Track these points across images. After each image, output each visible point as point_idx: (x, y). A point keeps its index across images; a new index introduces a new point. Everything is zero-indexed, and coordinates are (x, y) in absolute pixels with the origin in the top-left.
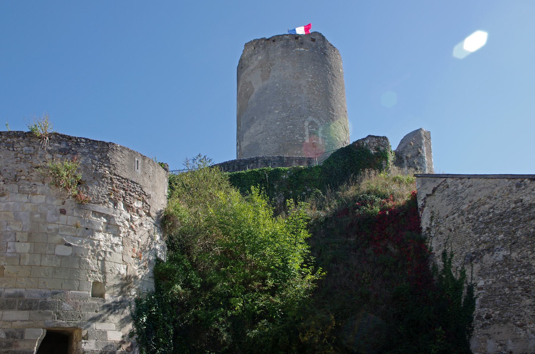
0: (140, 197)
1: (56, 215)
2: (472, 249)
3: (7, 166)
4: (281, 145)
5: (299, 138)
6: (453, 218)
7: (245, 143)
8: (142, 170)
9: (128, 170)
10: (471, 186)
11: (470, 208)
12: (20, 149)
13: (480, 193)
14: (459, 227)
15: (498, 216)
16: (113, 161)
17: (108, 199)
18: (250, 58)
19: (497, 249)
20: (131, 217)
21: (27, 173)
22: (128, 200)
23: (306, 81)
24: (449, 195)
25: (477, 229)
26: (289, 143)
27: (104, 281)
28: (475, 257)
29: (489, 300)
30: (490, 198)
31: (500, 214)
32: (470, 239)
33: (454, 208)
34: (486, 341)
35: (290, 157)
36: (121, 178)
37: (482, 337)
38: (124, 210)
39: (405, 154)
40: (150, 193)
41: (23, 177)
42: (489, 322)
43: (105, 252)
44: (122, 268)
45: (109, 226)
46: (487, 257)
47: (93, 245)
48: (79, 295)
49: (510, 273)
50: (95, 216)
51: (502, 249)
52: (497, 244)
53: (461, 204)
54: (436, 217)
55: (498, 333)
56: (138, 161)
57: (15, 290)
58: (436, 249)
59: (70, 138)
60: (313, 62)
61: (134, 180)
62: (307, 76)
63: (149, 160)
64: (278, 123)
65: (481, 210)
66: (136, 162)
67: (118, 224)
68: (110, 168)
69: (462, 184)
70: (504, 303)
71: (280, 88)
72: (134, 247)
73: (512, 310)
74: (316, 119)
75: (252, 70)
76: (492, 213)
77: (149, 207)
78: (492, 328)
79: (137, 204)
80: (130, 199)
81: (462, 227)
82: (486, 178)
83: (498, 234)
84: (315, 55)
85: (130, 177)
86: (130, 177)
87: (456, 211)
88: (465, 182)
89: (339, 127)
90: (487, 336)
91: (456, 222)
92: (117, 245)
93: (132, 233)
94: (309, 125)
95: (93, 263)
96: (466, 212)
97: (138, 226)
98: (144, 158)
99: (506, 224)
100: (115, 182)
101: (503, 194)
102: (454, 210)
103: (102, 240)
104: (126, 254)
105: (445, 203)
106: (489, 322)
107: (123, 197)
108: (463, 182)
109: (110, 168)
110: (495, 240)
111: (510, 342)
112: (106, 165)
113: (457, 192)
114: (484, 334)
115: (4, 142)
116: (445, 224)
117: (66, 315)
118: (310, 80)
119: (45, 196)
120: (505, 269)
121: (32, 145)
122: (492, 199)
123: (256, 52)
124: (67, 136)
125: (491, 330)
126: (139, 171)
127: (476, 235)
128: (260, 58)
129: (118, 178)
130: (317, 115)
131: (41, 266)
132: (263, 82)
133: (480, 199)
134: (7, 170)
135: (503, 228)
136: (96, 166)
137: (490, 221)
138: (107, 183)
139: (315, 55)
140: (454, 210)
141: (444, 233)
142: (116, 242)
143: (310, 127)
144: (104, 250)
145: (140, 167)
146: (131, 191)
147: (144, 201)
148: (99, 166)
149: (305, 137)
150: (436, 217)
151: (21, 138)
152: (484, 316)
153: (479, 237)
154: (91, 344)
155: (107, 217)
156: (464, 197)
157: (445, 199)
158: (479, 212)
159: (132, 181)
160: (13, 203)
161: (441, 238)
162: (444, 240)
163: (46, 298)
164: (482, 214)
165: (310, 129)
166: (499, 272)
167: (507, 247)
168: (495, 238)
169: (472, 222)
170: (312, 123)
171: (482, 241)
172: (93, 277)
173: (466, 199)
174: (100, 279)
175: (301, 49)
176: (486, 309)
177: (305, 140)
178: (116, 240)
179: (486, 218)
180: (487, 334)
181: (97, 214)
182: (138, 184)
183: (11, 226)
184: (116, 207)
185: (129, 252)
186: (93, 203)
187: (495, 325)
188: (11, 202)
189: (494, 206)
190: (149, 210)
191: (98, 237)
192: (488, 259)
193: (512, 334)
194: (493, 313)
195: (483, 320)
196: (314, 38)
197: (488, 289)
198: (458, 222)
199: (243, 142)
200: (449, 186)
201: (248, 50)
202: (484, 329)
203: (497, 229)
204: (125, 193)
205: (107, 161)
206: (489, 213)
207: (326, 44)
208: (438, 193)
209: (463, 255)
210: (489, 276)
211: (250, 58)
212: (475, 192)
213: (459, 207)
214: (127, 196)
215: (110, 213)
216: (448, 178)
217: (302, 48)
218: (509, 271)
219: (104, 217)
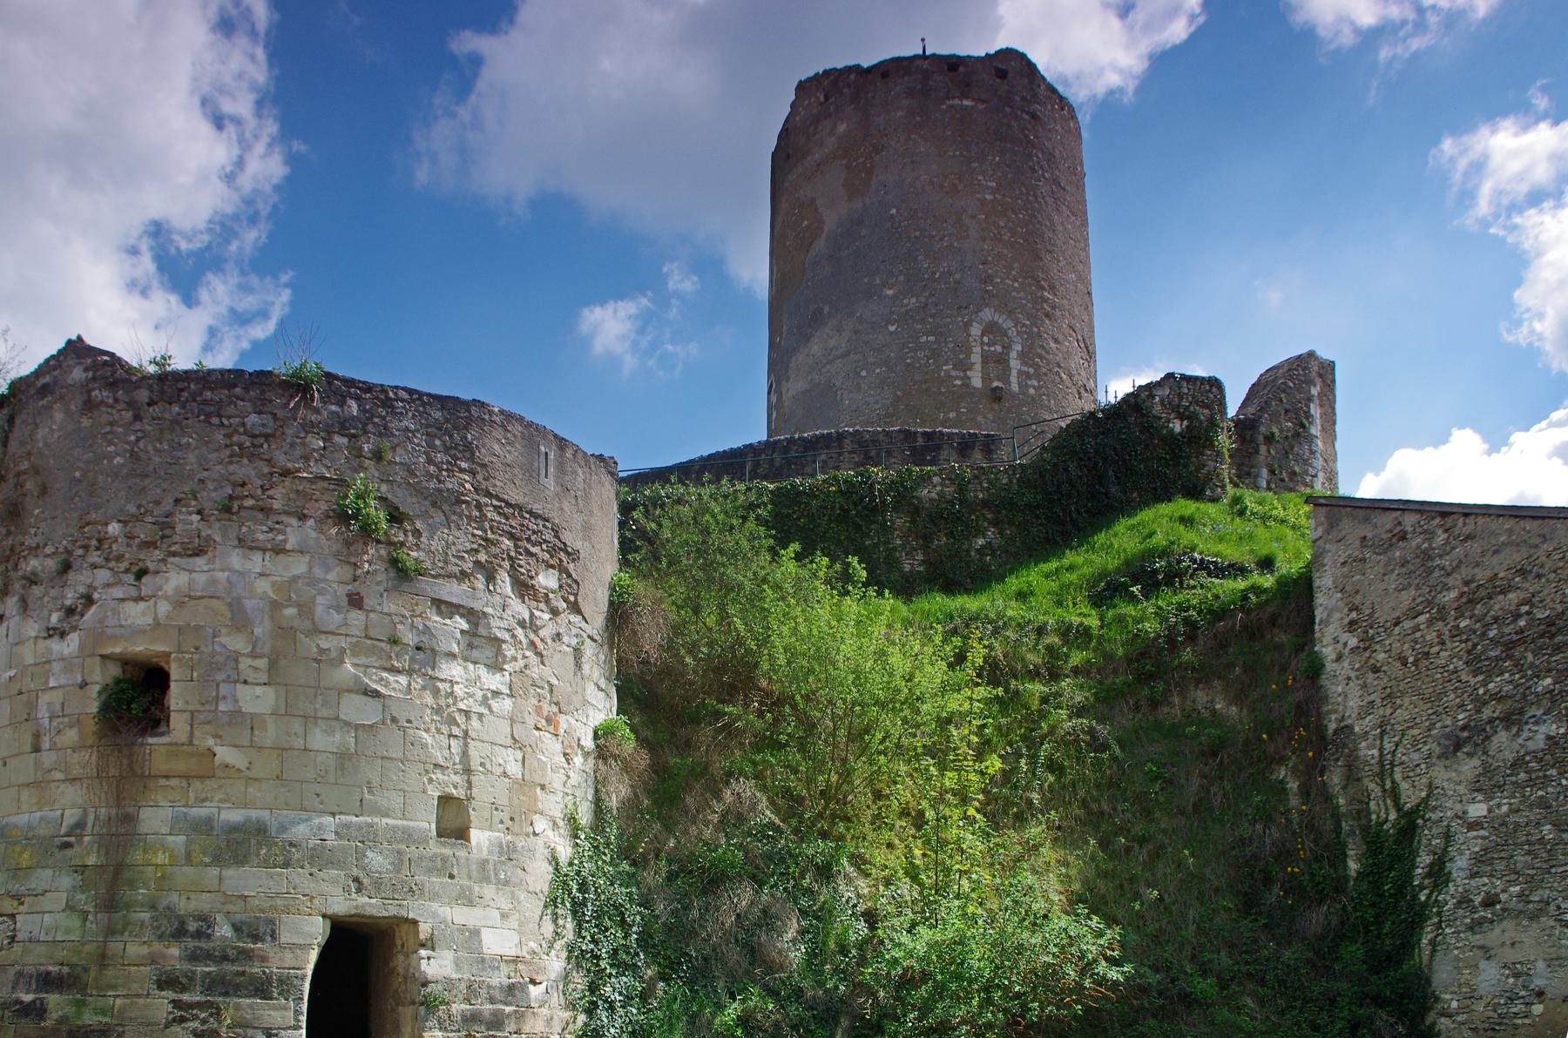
0: (552, 557)
1: (338, 609)
2: (1460, 717)
3: (207, 470)
5: (953, 373)
6: (1414, 627)
7: (795, 386)
8: (557, 477)
9: (522, 480)
10: (1469, 537)
11: (1464, 600)
12: (237, 420)
13: (1495, 559)
14: (1428, 653)
15: (1542, 627)
16: (482, 455)
17: (471, 565)
18: (813, 127)
19: (1530, 718)
20: (532, 615)
21: (259, 492)
22: (522, 567)
23: (978, 199)
24: (1408, 562)
25: (1480, 661)
26: (924, 386)
27: (466, 795)
28: (1469, 737)
29: (1496, 856)
30: (1522, 572)
31: (1548, 620)
32: (1456, 688)
33: (1420, 600)
34: (1476, 966)
35: (935, 432)
36: (503, 505)
37: (1467, 955)
38: (513, 596)
39: (1262, 429)
40: (578, 545)
41: (249, 502)
42: (1490, 916)
43: (467, 713)
44: (512, 758)
45: (476, 641)
46: (1501, 737)
47: (436, 692)
48: (405, 830)
49: (1560, 784)
50: (440, 613)
51: (1545, 717)
52: (1533, 704)
53: (1439, 589)
54: (1364, 624)
55: (1513, 944)
56: (546, 453)
58: (1359, 714)
59: (368, 388)
60: (998, 143)
61: (537, 508)
62: (979, 185)
63: (576, 451)
64: (892, 328)
65: (1497, 607)
66: (542, 458)
67: (499, 635)
68: (474, 474)
69: (1446, 531)
70: (1536, 865)
71: (900, 222)
72: (540, 701)
73: (1556, 885)
74: (1005, 317)
75: (818, 165)
76: (1525, 617)
77: (575, 587)
78: (1497, 931)
79: (547, 580)
80: (529, 564)
81: (1438, 653)
82: (1516, 517)
83: (1538, 677)
84: (1005, 121)
85: (526, 499)
86: (526, 499)
87: (1424, 608)
88: (1455, 526)
89: (1070, 342)
90: (1480, 953)
91: (1420, 640)
92: (496, 694)
93: (534, 659)
94: (983, 335)
95: (436, 744)
96: (1452, 613)
97: (549, 641)
98: (562, 443)
99: (1563, 650)
100: (489, 515)
101: (1561, 564)
102: (1418, 605)
103: (459, 680)
104: (520, 719)
105: (1392, 582)
106: (1490, 916)
107: (510, 558)
108: (1448, 525)
109: (474, 474)
110: (1528, 692)
111: (1541, 965)
112: (464, 465)
113: (1430, 552)
114: (1473, 947)
115: (195, 400)
116: (1390, 644)
117: (377, 884)
118: (989, 197)
119: (307, 558)
120: (1548, 773)
121: (269, 408)
122: (1530, 578)
123: (832, 109)
124: (359, 381)
125: (1494, 936)
126: (550, 483)
127: (1475, 677)
128: (842, 128)
129: (495, 502)
130: (1006, 305)
131: (305, 749)
133: (1496, 575)
134: (207, 481)
135: (1554, 658)
136: (438, 467)
137: (1519, 639)
138: (469, 518)
139: (1005, 121)
140: (1418, 605)
141: (1383, 669)
142: (493, 687)
143: (986, 339)
144: (465, 708)
145: (551, 470)
146: (528, 540)
147: (563, 570)
148: (447, 470)
149: (970, 369)
150: (1364, 624)
151: (238, 390)
152: (1478, 900)
153: (1484, 684)
154: (443, 963)
155: (471, 615)
156: (1449, 569)
157: (1393, 570)
158: (1488, 612)
159: (531, 513)
160: (226, 574)
161: (1376, 683)
162: (1384, 688)
163: (323, 837)
164: (1496, 619)
165: (986, 348)
166: (1531, 780)
167: (1560, 713)
168: (1529, 687)
169: (1467, 640)
170: (991, 329)
171: (1491, 695)
172: (439, 784)
173: (1455, 575)
174: (456, 787)
175: (966, 103)
176: (1486, 880)
177: (969, 378)
178: (495, 681)
179: (1507, 630)
180: (1482, 947)
181: (443, 607)
182: (548, 521)
183: (223, 640)
184: (491, 588)
185: (526, 714)
186: (434, 577)
187: (1505, 922)
188: (222, 570)
189: (1533, 596)
190: (576, 595)
191: (448, 672)
192: (1505, 745)
193: (1550, 947)
194: (1504, 891)
195: (1474, 910)
196: (1004, 68)
197: (1496, 826)
198: (1428, 638)
199: (787, 381)
200: (1409, 536)
201: (807, 102)
202: (1474, 933)
203: (1537, 663)
204: (516, 546)
205: (467, 455)
206: (1517, 616)
207: (1039, 86)
208: (1375, 553)
209: (1434, 732)
210: (1502, 792)
211: (813, 127)
212: (1483, 554)
213: (1434, 597)
214: (521, 554)
215: (477, 605)
216: (1406, 512)
217: (967, 98)
218: (1560, 780)
219: (462, 616)
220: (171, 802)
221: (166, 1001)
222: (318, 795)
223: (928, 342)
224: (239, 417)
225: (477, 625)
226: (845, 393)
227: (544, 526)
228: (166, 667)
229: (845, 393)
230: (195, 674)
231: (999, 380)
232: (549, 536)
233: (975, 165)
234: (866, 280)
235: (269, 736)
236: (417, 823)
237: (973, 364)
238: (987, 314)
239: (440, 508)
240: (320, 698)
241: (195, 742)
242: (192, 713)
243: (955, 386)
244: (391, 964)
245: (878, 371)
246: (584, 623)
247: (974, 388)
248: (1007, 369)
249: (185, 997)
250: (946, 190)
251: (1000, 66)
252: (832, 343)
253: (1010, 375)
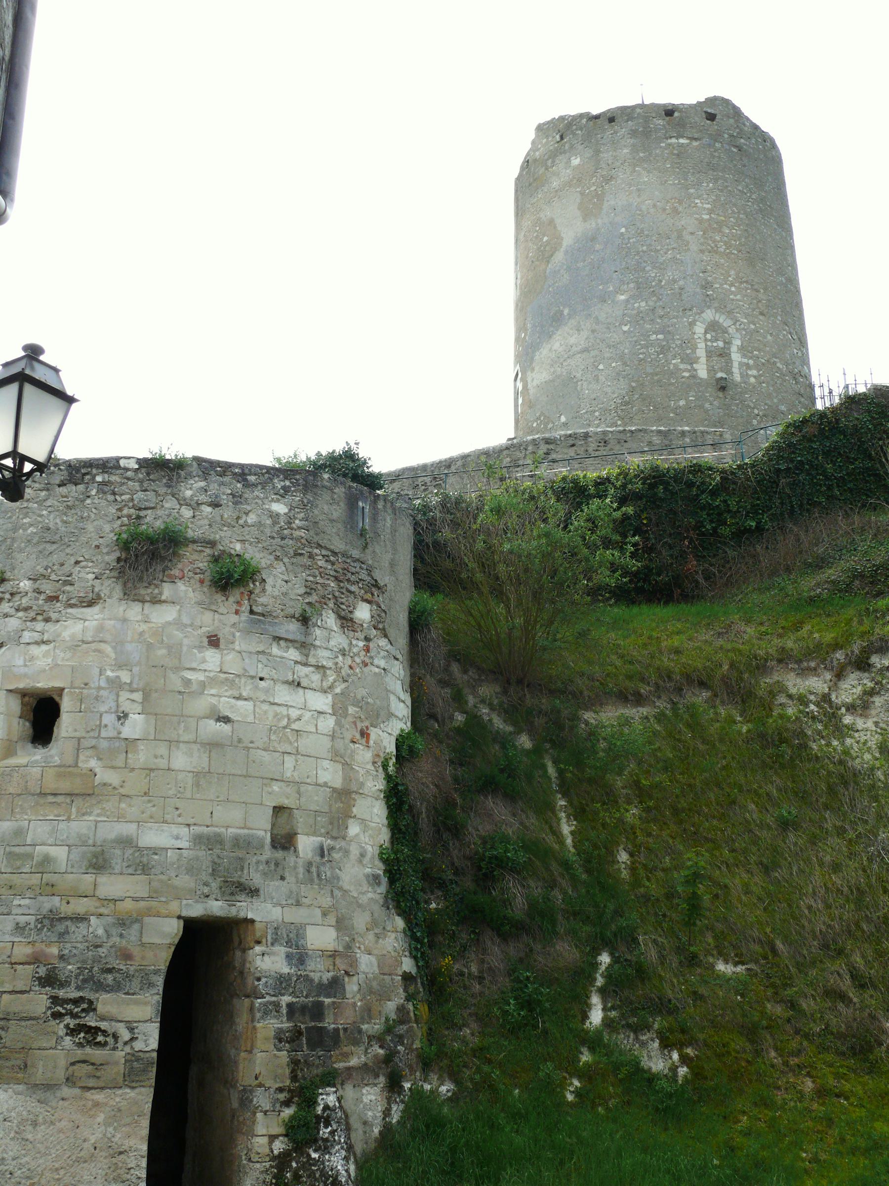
4: (634, 384)
5: (682, 366)
12: (128, 496)
23: (696, 219)
26: (656, 378)
64: (625, 328)
79: (363, 613)
84: (716, 154)
94: (706, 333)
130: (725, 307)
139: (716, 154)
143: (709, 336)
146: (348, 580)
149: (696, 362)
165: (709, 343)
170: (713, 327)
175: (682, 141)
177: (696, 370)
182: (363, 563)
188: (110, 619)
217: (682, 137)
220: (56, 816)
221: (45, 997)
222: (177, 809)
223: (658, 339)
224: (128, 494)
225: (307, 656)
226: (585, 384)
227: (360, 567)
228: (57, 698)
229: (585, 384)
230: (83, 707)
231: (722, 371)
232: (363, 575)
233: (692, 191)
234: (601, 287)
235: (141, 757)
236: (254, 831)
237: (699, 358)
238: (709, 315)
239: (282, 560)
240: (183, 724)
241: (80, 765)
242: (79, 739)
243: (683, 377)
244: (226, 958)
245: (614, 365)
246: (389, 646)
247: (701, 379)
248: (729, 361)
249: (61, 993)
250: (668, 212)
251: (709, 111)
252: (572, 340)
253: (732, 367)
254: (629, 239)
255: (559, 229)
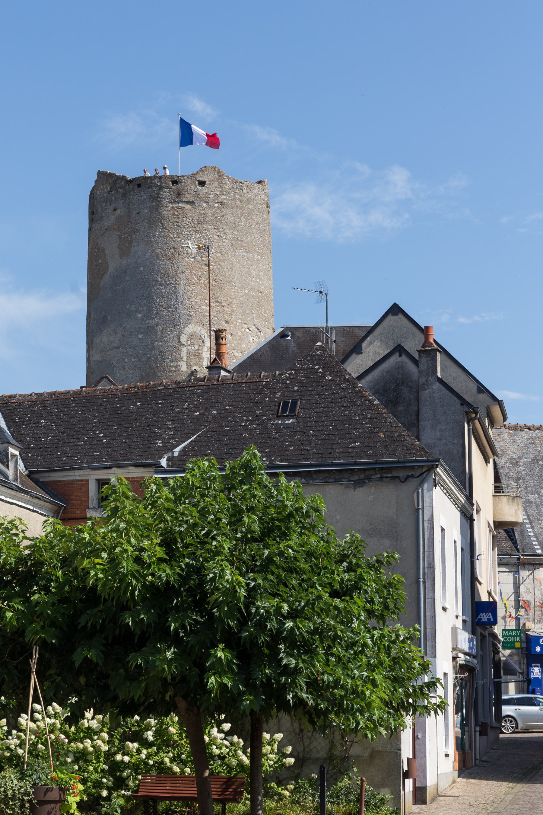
4: (144, 374)
15: (534, 500)
57: (80, 473)
64: (140, 336)
75: (106, 230)
132: (121, 258)
237: (181, 358)
251: (201, 179)
254: (145, 275)
255: (107, 258)
